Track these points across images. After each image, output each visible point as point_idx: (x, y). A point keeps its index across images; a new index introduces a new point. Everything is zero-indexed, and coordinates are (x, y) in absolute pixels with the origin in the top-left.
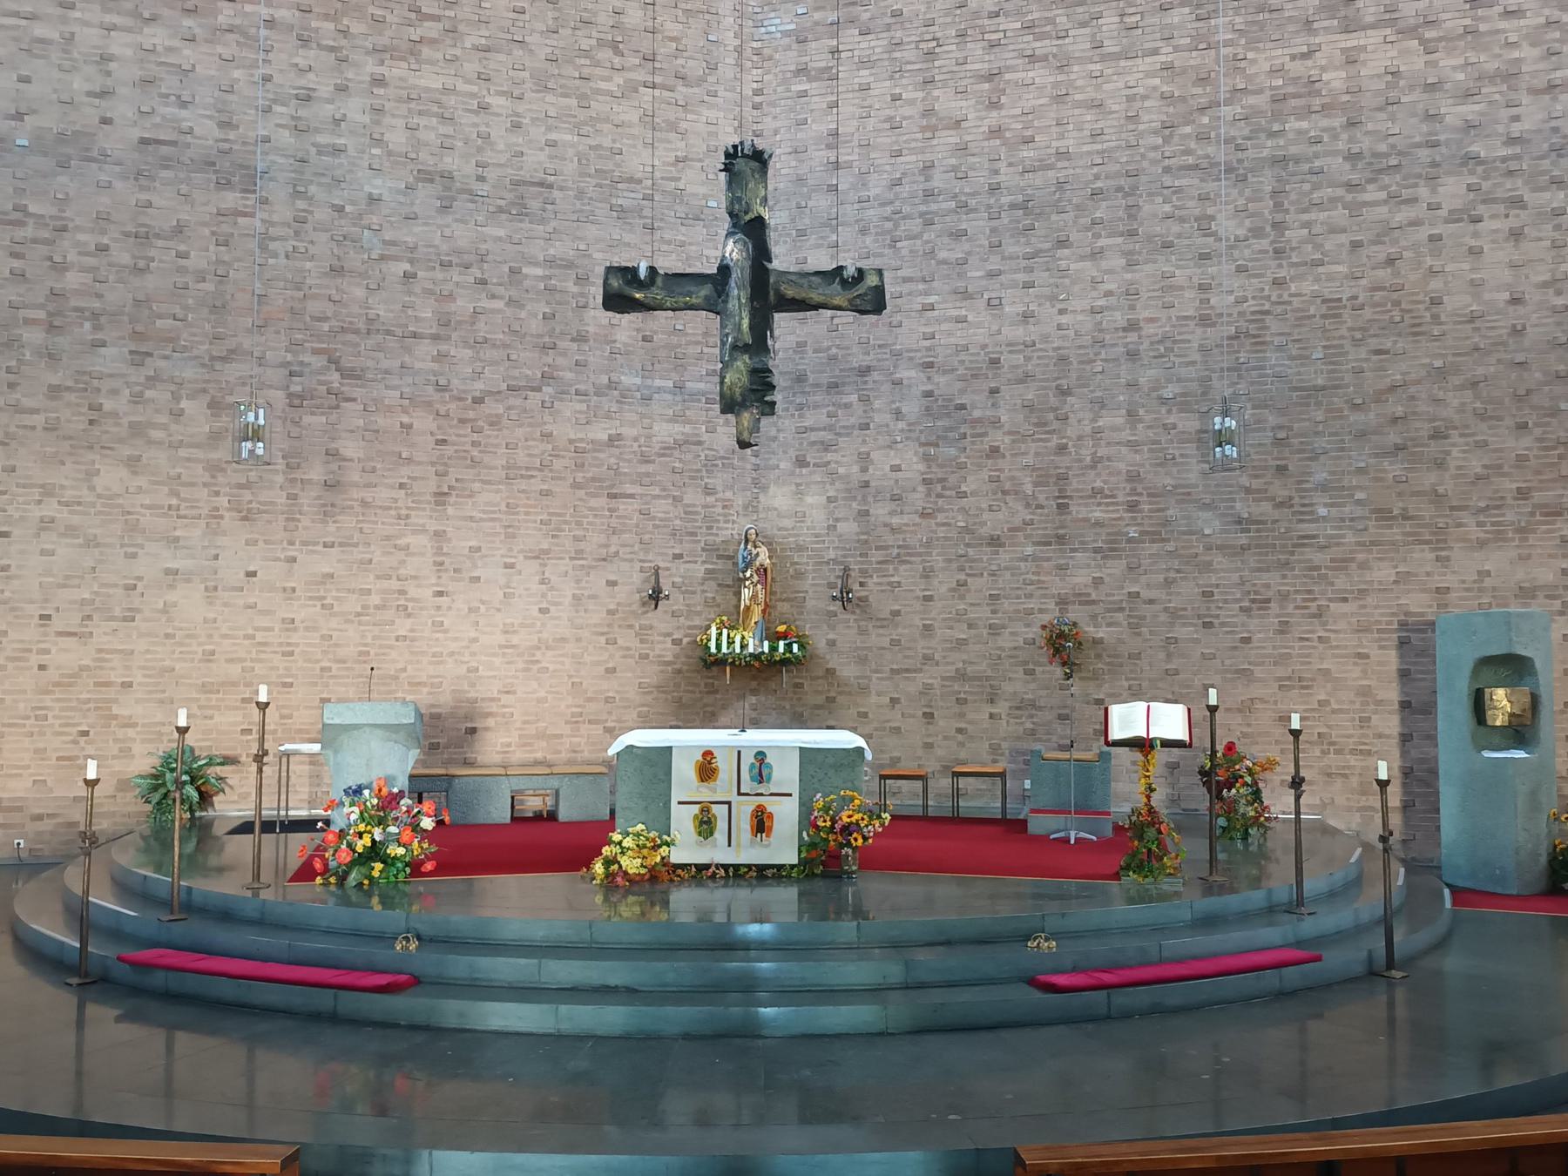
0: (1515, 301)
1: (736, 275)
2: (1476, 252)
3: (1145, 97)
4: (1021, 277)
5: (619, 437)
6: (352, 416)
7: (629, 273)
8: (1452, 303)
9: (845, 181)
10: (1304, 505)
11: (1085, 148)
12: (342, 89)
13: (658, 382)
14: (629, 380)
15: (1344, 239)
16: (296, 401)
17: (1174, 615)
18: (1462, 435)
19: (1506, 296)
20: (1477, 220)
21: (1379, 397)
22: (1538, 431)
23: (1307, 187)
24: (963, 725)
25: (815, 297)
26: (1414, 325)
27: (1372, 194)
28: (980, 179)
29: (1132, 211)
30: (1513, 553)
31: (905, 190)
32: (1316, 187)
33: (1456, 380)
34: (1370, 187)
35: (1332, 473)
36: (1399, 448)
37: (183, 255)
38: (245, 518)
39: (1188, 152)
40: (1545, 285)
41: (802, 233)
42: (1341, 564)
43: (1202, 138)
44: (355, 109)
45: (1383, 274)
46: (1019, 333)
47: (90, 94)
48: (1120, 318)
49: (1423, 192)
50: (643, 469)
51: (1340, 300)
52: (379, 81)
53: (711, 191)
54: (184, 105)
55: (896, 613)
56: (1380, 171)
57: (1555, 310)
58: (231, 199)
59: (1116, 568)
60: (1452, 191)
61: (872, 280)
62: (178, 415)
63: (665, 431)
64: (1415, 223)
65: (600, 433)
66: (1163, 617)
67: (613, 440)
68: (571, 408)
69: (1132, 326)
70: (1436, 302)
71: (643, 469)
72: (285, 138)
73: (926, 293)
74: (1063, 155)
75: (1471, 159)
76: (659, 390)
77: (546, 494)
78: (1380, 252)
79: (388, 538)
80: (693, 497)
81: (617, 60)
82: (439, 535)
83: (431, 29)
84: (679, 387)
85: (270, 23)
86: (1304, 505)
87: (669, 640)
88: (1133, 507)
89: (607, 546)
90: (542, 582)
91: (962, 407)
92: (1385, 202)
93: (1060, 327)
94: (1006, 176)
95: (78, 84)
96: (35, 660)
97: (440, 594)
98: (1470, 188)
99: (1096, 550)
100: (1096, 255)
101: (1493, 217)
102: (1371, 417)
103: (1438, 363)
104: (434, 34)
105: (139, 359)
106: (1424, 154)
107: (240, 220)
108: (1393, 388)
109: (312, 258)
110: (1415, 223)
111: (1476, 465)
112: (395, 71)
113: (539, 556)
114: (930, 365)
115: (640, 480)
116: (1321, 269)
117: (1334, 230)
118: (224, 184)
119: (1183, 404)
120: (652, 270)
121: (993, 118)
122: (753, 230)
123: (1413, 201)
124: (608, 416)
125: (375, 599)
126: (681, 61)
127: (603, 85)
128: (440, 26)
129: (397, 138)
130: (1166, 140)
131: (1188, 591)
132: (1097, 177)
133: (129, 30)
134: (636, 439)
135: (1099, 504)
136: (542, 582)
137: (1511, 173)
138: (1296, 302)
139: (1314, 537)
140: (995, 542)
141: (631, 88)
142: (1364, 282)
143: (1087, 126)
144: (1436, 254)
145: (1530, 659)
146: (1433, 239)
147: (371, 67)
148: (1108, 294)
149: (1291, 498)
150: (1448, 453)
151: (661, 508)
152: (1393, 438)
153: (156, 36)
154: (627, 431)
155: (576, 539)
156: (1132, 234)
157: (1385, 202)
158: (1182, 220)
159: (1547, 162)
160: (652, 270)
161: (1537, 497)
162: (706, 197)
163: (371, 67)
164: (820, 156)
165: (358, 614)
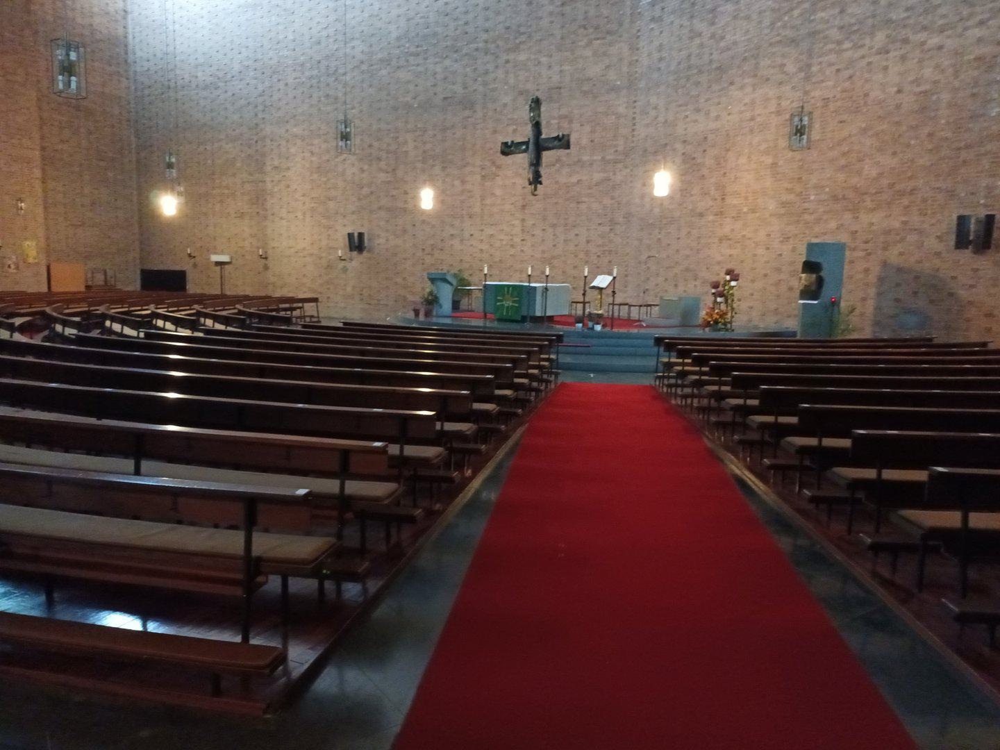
0: (899, 91)
1: (531, 141)
2: (886, 68)
3: (765, 11)
4: (716, 100)
5: (580, 180)
6: (499, 181)
7: (505, 144)
8: (873, 95)
9: (663, 65)
10: (807, 195)
11: (743, 39)
12: (497, 67)
13: (595, 158)
14: (585, 158)
15: (834, 68)
16: (484, 177)
17: (757, 244)
18: (870, 159)
19: (895, 89)
20: (887, 52)
21: (839, 143)
22: (901, 155)
23: (821, 45)
24: (686, 289)
25: (550, 145)
26: (857, 108)
27: (847, 45)
28: (706, 58)
29: (757, 65)
30: (884, 214)
31: (682, 67)
32: (826, 44)
33: (870, 133)
34: (846, 42)
35: (819, 180)
36: (843, 167)
37: (454, 134)
38: (470, 217)
39: (778, 35)
40: (913, 82)
41: (649, 89)
42: (818, 221)
43: (784, 27)
44: (500, 74)
45: (847, 84)
46: (713, 125)
47: (432, 86)
48: (748, 115)
49: (867, 41)
50: (589, 191)
51: (828, 98)
52: (507, 62)
53: (525, 113)
54: (454, 84)
55: (669, 245)
56: (850, 33)
57: (915, 94)
58: (467, 113)
59: (738, 225)
60: (880, 37)
61: (566, 138)
62: (453, 186)
63: (598, 176)
64: (863, 57)
65: (574, 179)
66: (753, 245)
67: (579, 181)
68: (565, 171)
69: (752, 119)
70: (866, 95)
71: (589, 191)
72: (481, 89)
73: (686, 111)
74: (735, 43)
75: (890, 21)
76: (595, 161)
77: (556, 203)
78: (846, 73)
79: (508, 222)
80: (607, 201)
81: (585, 32)
82: (523, 220)
83: (523, 38)
84: (603, 158)
85: (477, 50)
86: (807, 195)
87: (596, 255)
88: (746, 198)
89: (575, 221)
90: (554, 235)
91: (694, 158)
92: (851, 48)
93: (728, 121)
94: (715, 56)
95: (429, 84)
96: (421, 261)
97: (523, 240)
98: (888, 36)
99: (733, 217)
100: (742, 88)
101: (895, 50)
102: (835, 153)
103: (864, 125)
104: (524, 40)
105: (444, 168)
106: (870, 21)
107: (469, 119)
108: (845, 139)
109: (487, 129)
110: (863, 57)
111: (874, 173)
112: (511, 57)
113: (554, 226)
114: (685, 142)
115: (590, 195)
116: (824, 84)
117: (831, 65)
118: (466, 108)
119: (766, 153)
120: (512, 142)
121: (713, 29)
122: (537, 126)
123: (862, 46)
124: (578, 172)
125: (504, 243)
126: (609, 26)
127: (580, 44)
128: (526, 36)
129: (512, 81)
130: (772, 29)
131: (762, 235)
132: (745, 51)
133: (440, 62)
134: (587, 180)
135: (736, 198)
136: (554, 235)
137: (905, 26)
138: (813, 101)
139: (809, 209)
140: (701, 215)
141: (590, 43)
142: (839, 89)
143: (744, 28)
144: (870, 71)
145: (819, 263)
146: (869, 64)
147: (505, 57)
148: (745, 104)
149: (802, 192)
150: (863, 168)
151: (595, 206)
152: (843, 162)
153: (447, 62)
154: (584, 178)
155: (566, 219)
156: (756, 76)
157: (851, 48)
158: (774, 67)
159: (922, 17)
160: (512, 142)
161: (898, 187)
162: (616, 80)
163: (505, 57)
164: (656, 55)
165: (500, 248)
